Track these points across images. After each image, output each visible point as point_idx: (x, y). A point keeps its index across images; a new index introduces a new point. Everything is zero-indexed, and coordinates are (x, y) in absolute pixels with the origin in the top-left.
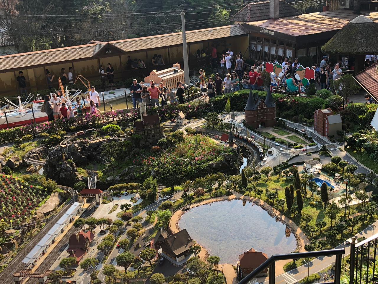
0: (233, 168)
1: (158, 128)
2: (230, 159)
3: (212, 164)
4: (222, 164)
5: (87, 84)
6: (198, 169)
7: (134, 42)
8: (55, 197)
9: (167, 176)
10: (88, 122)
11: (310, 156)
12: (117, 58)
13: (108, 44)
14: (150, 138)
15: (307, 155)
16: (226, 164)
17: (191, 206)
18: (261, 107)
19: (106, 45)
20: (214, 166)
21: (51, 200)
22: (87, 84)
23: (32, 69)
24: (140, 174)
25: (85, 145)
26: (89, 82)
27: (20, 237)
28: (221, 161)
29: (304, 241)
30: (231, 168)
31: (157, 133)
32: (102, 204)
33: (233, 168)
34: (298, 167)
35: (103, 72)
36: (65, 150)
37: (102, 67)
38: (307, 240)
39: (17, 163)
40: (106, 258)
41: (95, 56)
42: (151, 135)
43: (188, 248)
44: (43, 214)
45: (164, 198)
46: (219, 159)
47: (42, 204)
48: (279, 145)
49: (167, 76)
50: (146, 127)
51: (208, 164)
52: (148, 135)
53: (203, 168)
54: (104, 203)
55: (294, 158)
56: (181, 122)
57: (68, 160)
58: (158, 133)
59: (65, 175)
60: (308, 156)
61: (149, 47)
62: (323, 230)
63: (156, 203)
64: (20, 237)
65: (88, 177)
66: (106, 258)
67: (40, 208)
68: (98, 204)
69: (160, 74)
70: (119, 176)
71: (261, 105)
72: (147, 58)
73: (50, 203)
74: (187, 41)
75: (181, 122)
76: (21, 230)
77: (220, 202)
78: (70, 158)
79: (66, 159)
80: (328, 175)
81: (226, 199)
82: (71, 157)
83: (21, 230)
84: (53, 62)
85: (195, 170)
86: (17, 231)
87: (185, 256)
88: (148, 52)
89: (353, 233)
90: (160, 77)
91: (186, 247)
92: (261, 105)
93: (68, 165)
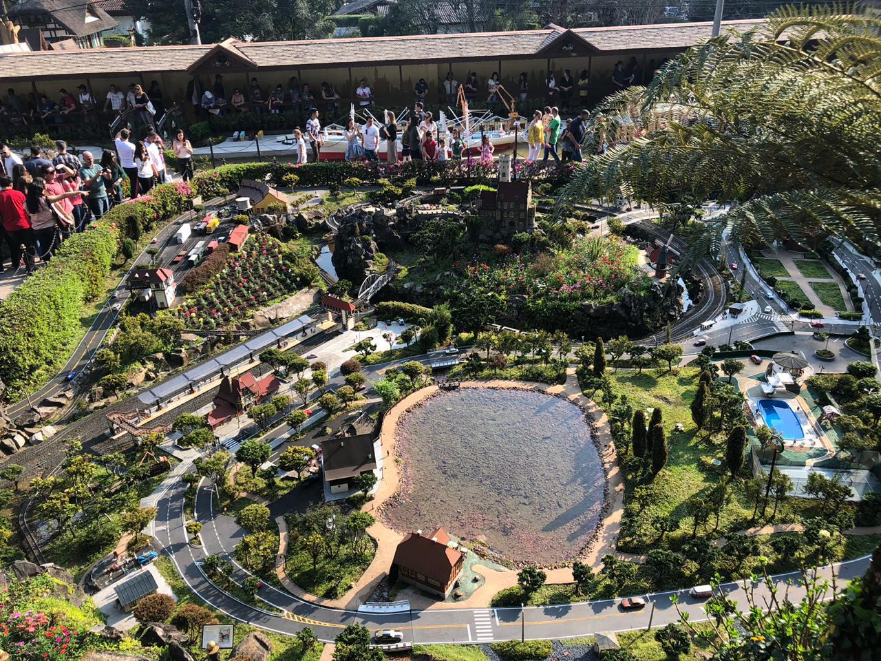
0: (636, 323)
1: (522, 210)
2: (633, 304)
3: (590, 306)
4: (611, 311)
5: (510, 104)
6: (556, 309)
7: (626, 33)
8: (308, 295)
10: (468, 173)
11: (818, 343)
12: (585, 60)
15: (815, 339)
16: (621, 312)
17: (462, 385)
19: (565, 33)
20: (592, 311)
22: (510, 104)
23: (436, 65)
25: (407, 216)
26: (513, 101)
27: (200, 350)
28: (611, 303)
29: (603, 547)
30: (629, 323)
31: (520, 220)
32: (352, 330)
33: (636, 323)
34: (761, 361)
35: (552, 84)
37: (552, 76)
41: (540, 52)
42: (508, 221)
43: (357, 474)
44: (267, 320)
46: (610, 298)
47: (275, 303)
48: (772, 299)
50: (499, 203)
51: (582, 305)
52: (502, 220)
54: (356, 329)
55: (777, 338)
59: (353, 260)
60: (815, 342)
62: (668, 537)
63: (428, 356)
64: (200, 350)
65: (381, 274)
68: (345, 328)
70: (423, 285)
73: (291, 304)
80: (815, 402)
81: (539, 391)
82: (373, 232)
86: (198, 337)
87: (349, 487)
88: (502, 62)
89: (734, 574)
91: (355, 470)
93: (359, 245)
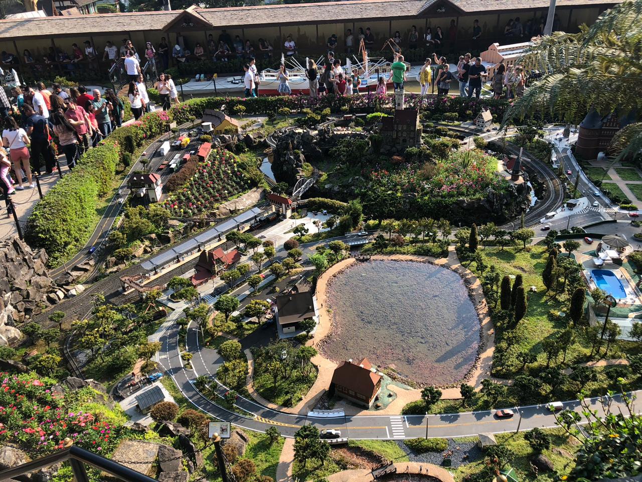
3: (463, 201)
6: (438, 203)
8: (256, 193)
9: (372, 205)
13: (187, 17)
14: (399, 143)
15: (633, 225)
16: (487, 206)
17: (372, 258)
18: (609, 126)
20: (465, 205)
21: (249, 196)
24: (360, 191)
27: (182, 232)
29: (481, 374)
30: (493, 214)
31: (411, 138)
32: (290, 218)
34: (592, 242)
36: (297, 136)
38: (488, 373)
39: (257, 140)
40: (230, 292)
42: (401, 139)
43: (301, 320)
45: (360, 234)
46: (478, 196)
47: (233, 199)
48: (598, 196)
49: (507, 55)
51: (457, 200)
53: (446, 204)
54: (292, 217)
55: (604, 225)
56: (482, 126)
57: (295, 150)
58: (412, 138)
60: (633, 227)
61: (503, 8)
62: (528, 367)
64: (182, 232)
66: (230, 292)
67: (226, 203)
69: (503, 50)
71: (610, 122)
72: (390, 32)
73: (244, 200)
74: (557, 4)
75: (482, 126)
76: (185, 224)
77: (419, 264)
78: (298, 149)
79: (294, 148)
81: (429, 262)
82: (301, 147)
83: (185, 224)
84: (365, 17)
85: (432, 203)
86: (180, 223)
90: (501, 54)
92: (610, 122)
93: (292, 157)
